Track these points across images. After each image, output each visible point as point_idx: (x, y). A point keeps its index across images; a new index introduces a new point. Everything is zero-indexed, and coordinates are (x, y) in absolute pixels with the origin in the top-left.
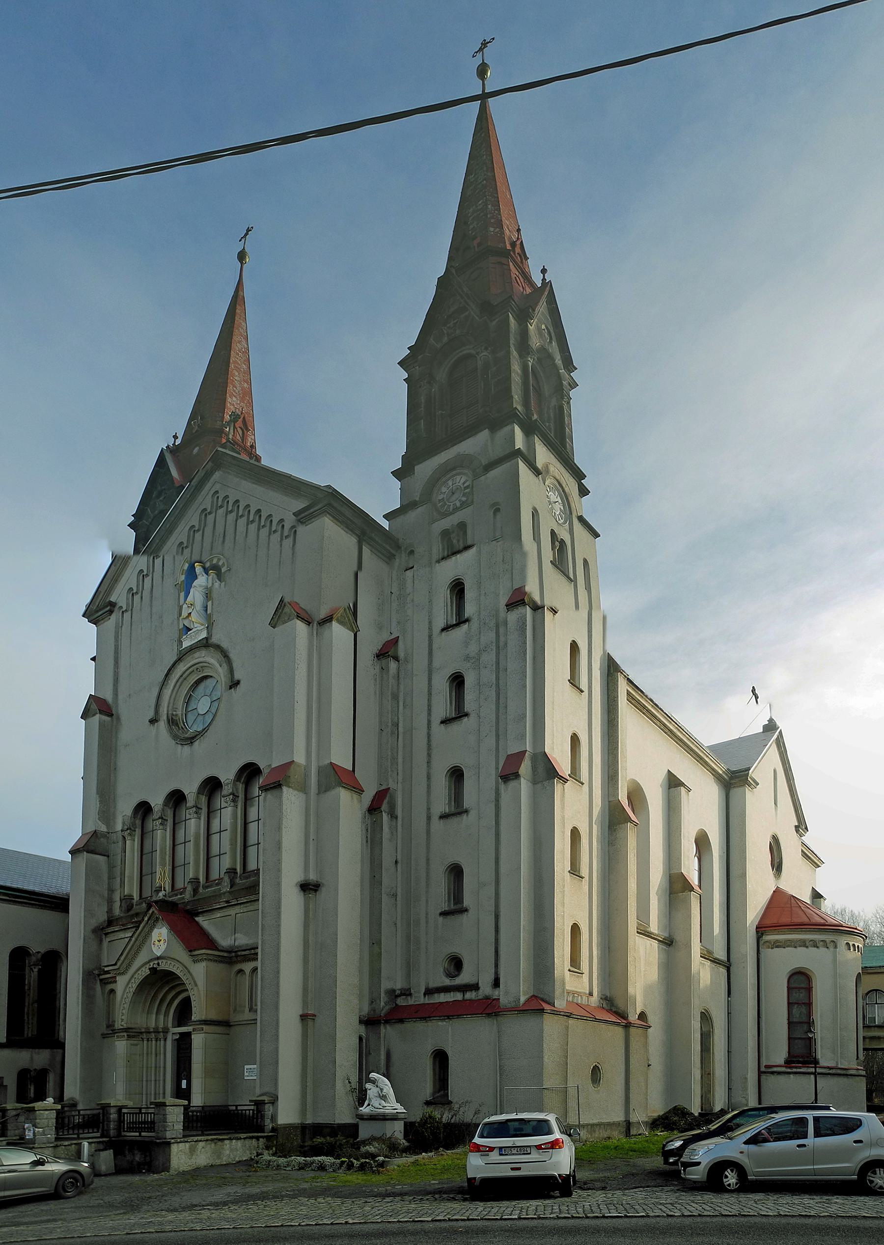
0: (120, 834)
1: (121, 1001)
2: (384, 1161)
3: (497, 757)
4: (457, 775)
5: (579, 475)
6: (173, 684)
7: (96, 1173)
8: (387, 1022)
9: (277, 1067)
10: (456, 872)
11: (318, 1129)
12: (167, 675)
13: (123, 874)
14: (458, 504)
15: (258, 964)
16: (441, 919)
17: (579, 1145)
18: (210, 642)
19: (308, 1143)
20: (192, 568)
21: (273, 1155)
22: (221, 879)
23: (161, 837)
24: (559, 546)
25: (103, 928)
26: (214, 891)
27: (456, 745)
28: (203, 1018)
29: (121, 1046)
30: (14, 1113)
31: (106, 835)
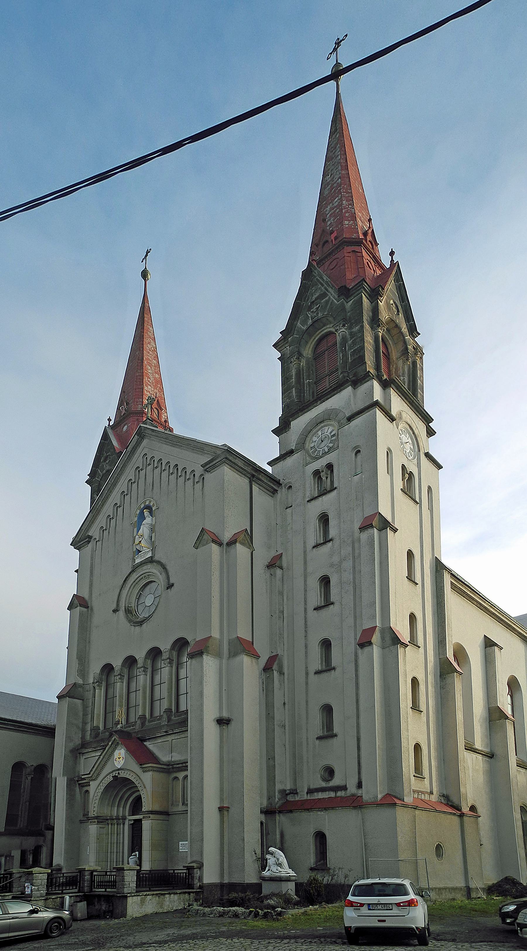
0: (91, 686)
1: (93, 798)
2: (281, 911)
3: (355, 631)
4: (326, 644)
5: (427, 419)
6: (129, 586)
7: (74, 919)
8: (280, 812)
9: (202, 843)
10: (328, 710)
11: (232, 887)
12: (125, 581)
13: (93, 713)
14: (326, 450)
15: (188, 773)
16: (317, 742)
17: (429, 903)
18: (154, 559)
19: (226, 897)
20: (142, 513)
21: (200, 905)
22: (161, 716)
23: (119, 687)
24: (408, 477)
25: (78, 749)
26: (156, 724)
27: (325, 624)
28: (150, 809)
29: (93, 828)
30: (18, 875)
31: (81, 686)
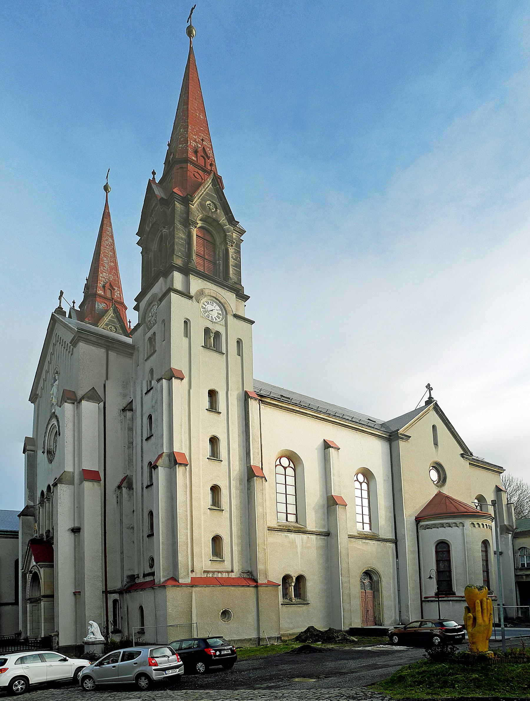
31: (32, 507)
